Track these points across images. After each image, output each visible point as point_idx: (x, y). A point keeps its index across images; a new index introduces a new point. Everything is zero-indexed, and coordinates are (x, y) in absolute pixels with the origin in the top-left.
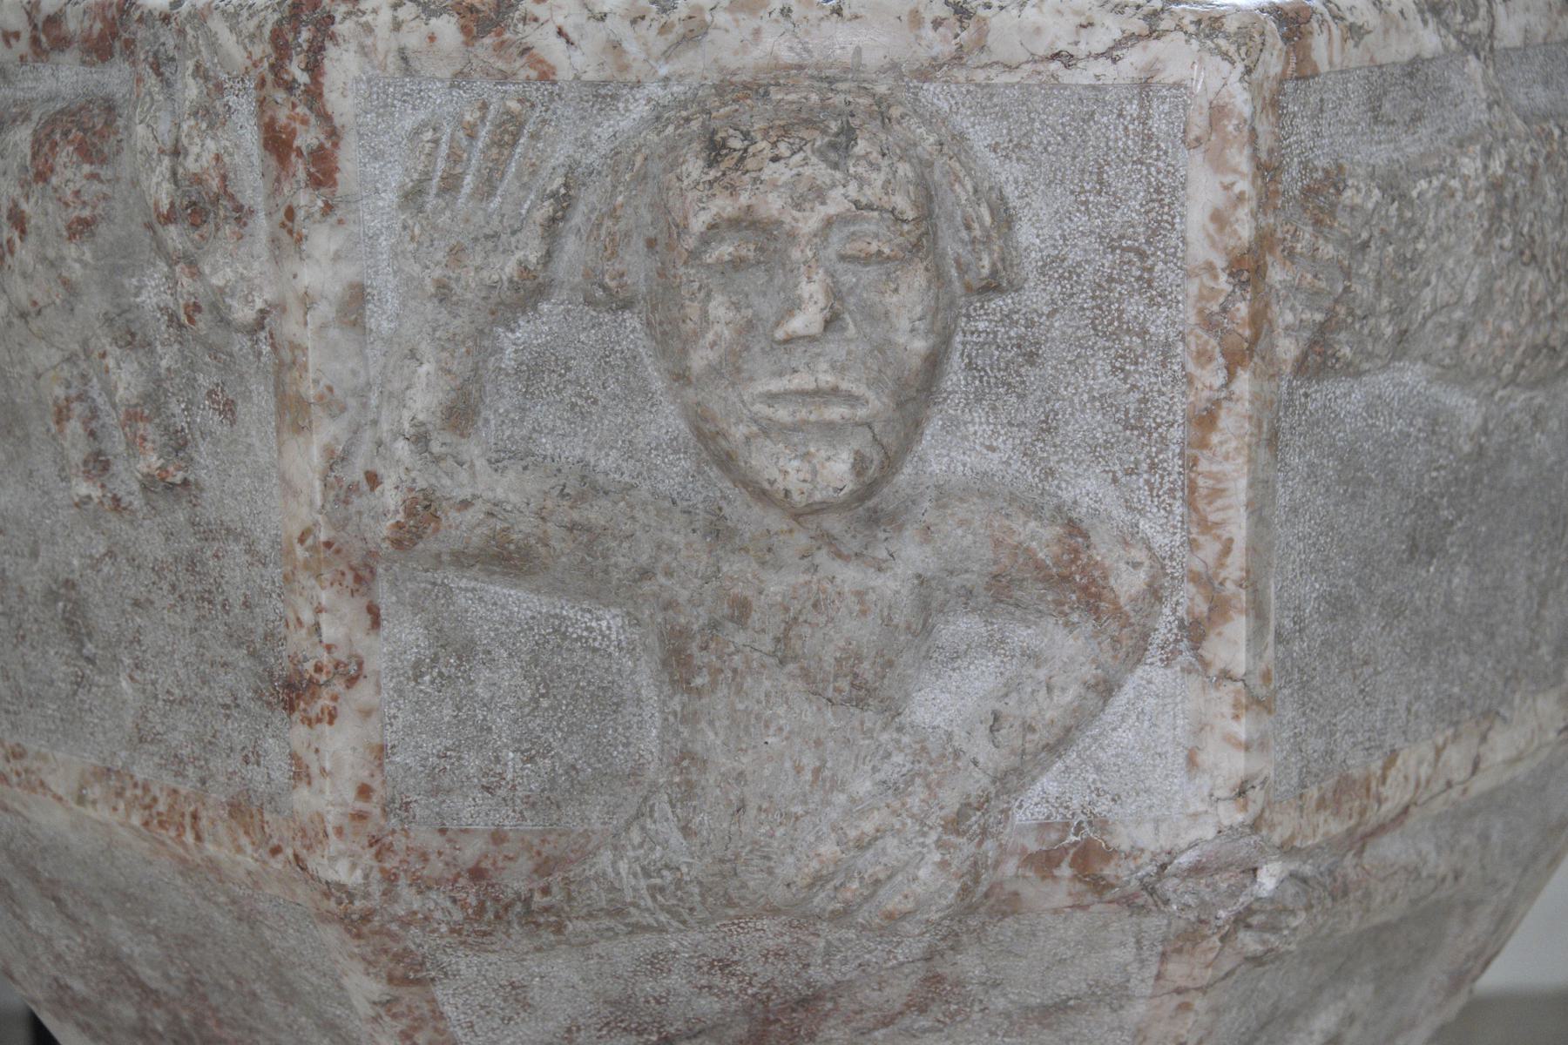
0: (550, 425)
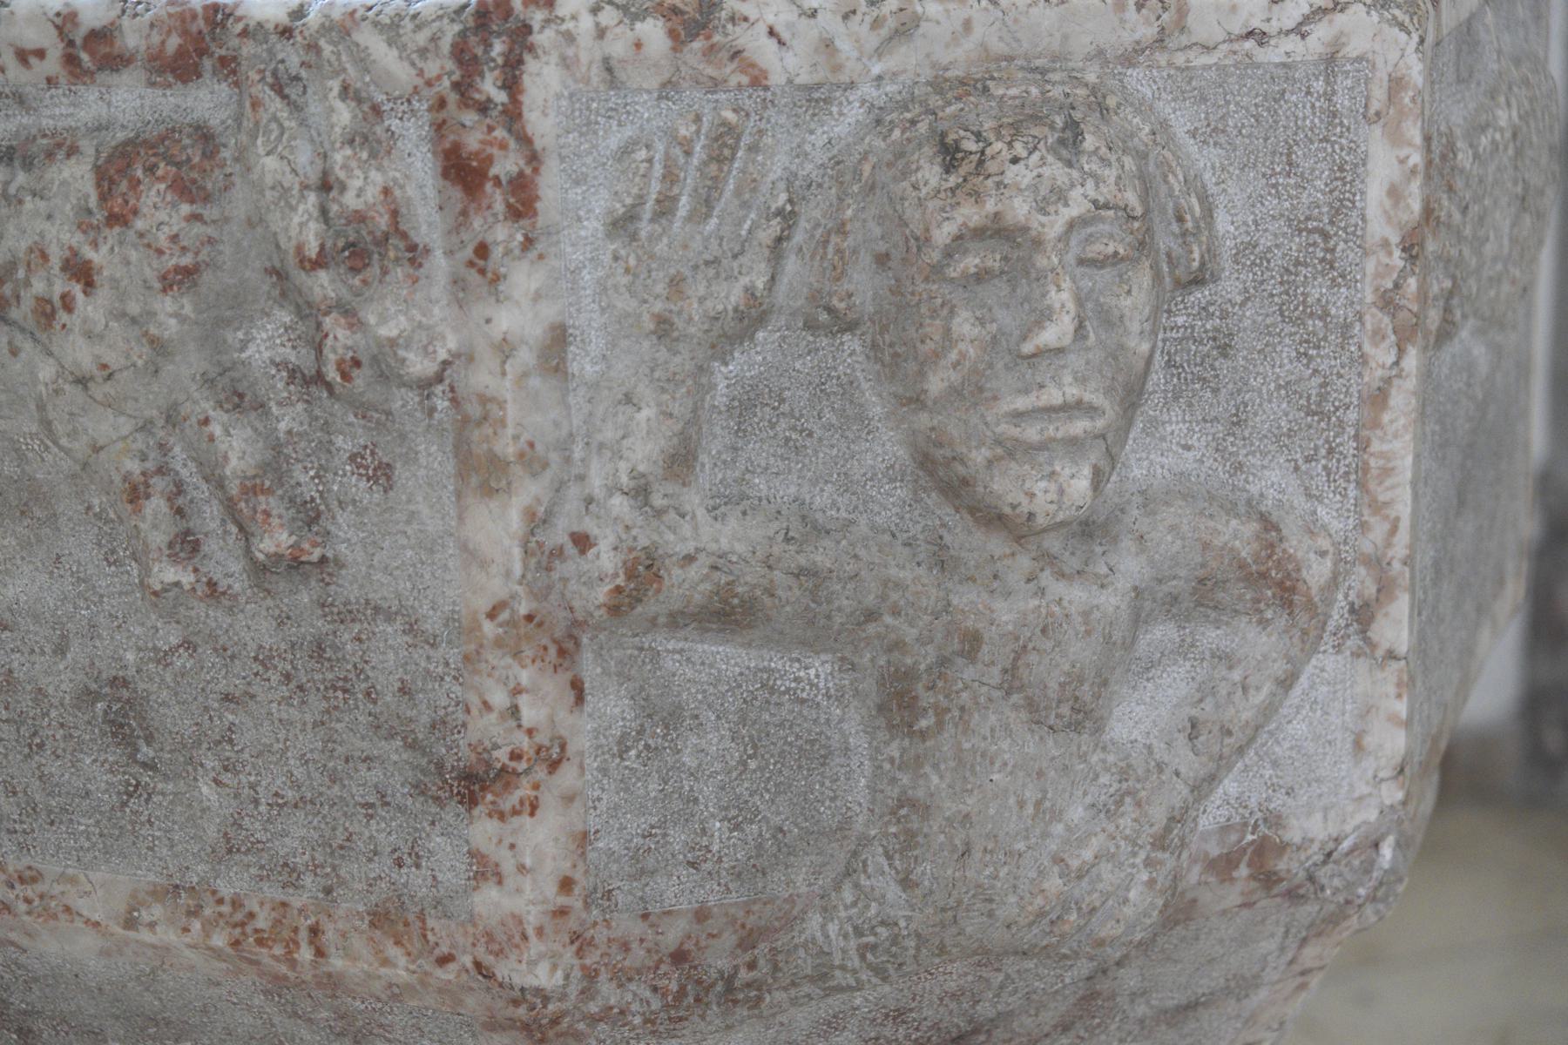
0: (763, 464)
